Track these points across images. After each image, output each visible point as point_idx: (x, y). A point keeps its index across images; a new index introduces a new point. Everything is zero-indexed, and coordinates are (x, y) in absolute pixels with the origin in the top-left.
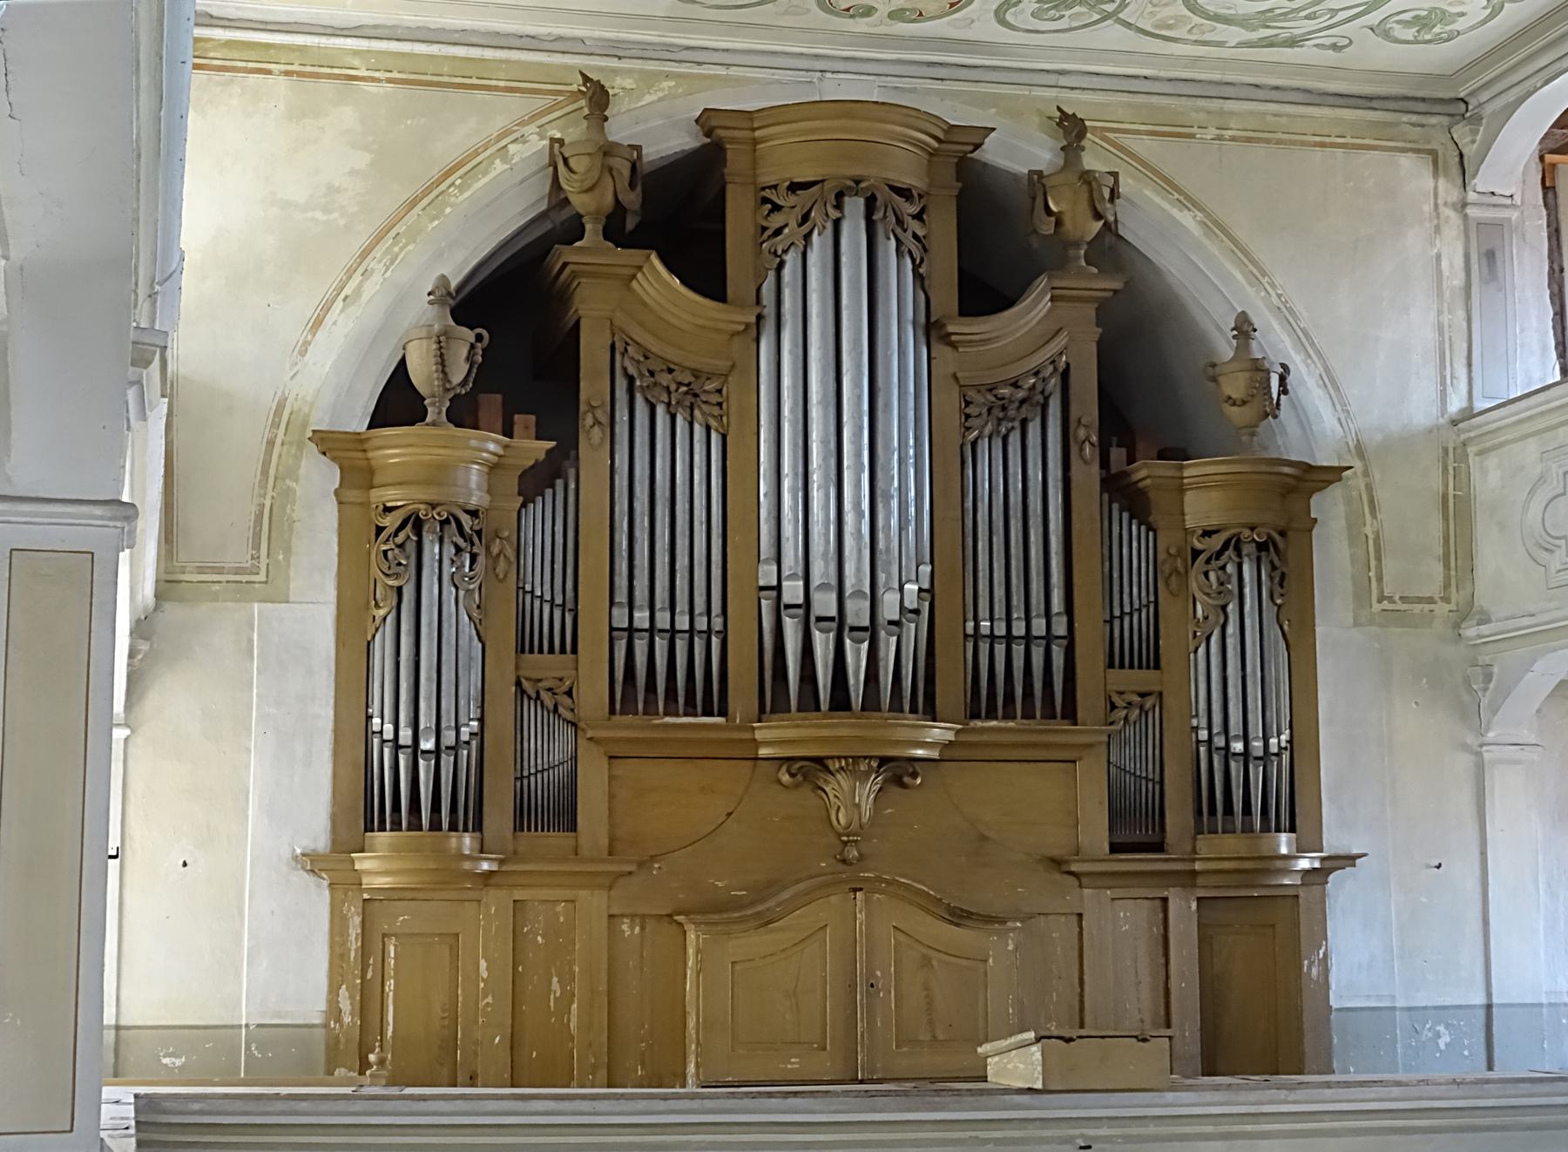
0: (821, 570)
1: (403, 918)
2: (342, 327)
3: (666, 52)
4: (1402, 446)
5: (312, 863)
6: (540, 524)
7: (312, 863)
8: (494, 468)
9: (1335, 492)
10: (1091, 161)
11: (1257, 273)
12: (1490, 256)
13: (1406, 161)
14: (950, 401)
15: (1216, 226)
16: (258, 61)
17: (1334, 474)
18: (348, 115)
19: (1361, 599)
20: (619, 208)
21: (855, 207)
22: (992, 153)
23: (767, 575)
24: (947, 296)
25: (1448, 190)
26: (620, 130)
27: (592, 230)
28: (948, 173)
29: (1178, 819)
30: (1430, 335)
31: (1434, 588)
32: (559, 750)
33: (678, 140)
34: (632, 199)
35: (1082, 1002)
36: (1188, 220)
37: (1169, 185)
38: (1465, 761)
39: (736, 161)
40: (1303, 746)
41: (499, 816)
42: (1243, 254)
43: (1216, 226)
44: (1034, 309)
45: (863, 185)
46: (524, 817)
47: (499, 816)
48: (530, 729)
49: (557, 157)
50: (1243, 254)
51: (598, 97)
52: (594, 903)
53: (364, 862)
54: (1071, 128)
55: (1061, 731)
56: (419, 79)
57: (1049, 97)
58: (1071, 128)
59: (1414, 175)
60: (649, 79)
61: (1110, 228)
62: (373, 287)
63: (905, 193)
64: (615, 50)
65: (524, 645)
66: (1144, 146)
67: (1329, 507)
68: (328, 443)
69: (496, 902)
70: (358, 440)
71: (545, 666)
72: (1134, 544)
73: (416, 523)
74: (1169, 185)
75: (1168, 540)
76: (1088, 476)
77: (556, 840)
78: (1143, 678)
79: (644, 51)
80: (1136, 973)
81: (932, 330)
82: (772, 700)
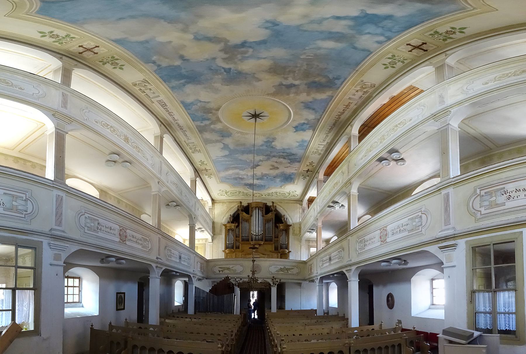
0: (257, 232)
1: (229, 255)
2: (225, 218)
3: (245, 199)
4: (296, 224)
5: (223, 251)
6: (237, 230)
7: (223, 251)
8: (234, 226)
9: (291, 227)
10: (274, 205)
11: (286, 212)
12: (304, 211)
13: (298, 205)
14: (264, 220)
15: (283, 209)
16: (220, 202)
17: (291, 225)
18: (225, 205)
19: (293, 234)
20: (242, 209)
21: (257, 208)
22: (268, 204)
23: (252, 232)
24: (264, 213)
25: (301, 206)
26: (242, 204)
27: (240, 211)
28: (264, 206)
29: (279, 248)
30: (299, 216)
31: (298, 233)
32: (238, 244)
33: (247, 205)
34: (243, 209)
35: (500, 107)
36: (282, 208)
37: (280, 206)
38: (300, 245)
39: (250, 206)
40: (288, 244)
41: (235, 248)
42: (285, 211)
43: (283, 209)
44: (270, 214)
45: (315, 321)
46: (236, 248)
47: (235, 248)
48: (237, 243)
49: (238, 206)
50: (285, 211)
51: (241, 203)
52: (240, 254)
53: (226, 251)
54: (273, 203)
55: (272, 242)
56: (230, 202)
57: (272, 201)
58: (273, 203)
59: (298, 205)
60: (245, 201)
61: (276, 209)
62: (227, 215)
63: (261, 207)
64: (242, 199)
65: (236, 237)
66: (279, 204)
67: (291, 228)
68: (224, 225)
69: (234, 254)
70: (226, 225)
71: (237, 239)
72: (277, 230)
73: (229, 230)
74: (280, 206)
75: (279, 229)
76: (274, 225)
77: (238, 250)
78: (277, 239)
79: (244, 199)
80: (380, 169)
81: (263, 216)
82: (252, 240)
